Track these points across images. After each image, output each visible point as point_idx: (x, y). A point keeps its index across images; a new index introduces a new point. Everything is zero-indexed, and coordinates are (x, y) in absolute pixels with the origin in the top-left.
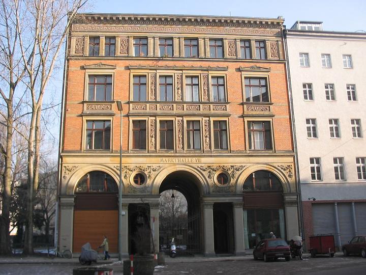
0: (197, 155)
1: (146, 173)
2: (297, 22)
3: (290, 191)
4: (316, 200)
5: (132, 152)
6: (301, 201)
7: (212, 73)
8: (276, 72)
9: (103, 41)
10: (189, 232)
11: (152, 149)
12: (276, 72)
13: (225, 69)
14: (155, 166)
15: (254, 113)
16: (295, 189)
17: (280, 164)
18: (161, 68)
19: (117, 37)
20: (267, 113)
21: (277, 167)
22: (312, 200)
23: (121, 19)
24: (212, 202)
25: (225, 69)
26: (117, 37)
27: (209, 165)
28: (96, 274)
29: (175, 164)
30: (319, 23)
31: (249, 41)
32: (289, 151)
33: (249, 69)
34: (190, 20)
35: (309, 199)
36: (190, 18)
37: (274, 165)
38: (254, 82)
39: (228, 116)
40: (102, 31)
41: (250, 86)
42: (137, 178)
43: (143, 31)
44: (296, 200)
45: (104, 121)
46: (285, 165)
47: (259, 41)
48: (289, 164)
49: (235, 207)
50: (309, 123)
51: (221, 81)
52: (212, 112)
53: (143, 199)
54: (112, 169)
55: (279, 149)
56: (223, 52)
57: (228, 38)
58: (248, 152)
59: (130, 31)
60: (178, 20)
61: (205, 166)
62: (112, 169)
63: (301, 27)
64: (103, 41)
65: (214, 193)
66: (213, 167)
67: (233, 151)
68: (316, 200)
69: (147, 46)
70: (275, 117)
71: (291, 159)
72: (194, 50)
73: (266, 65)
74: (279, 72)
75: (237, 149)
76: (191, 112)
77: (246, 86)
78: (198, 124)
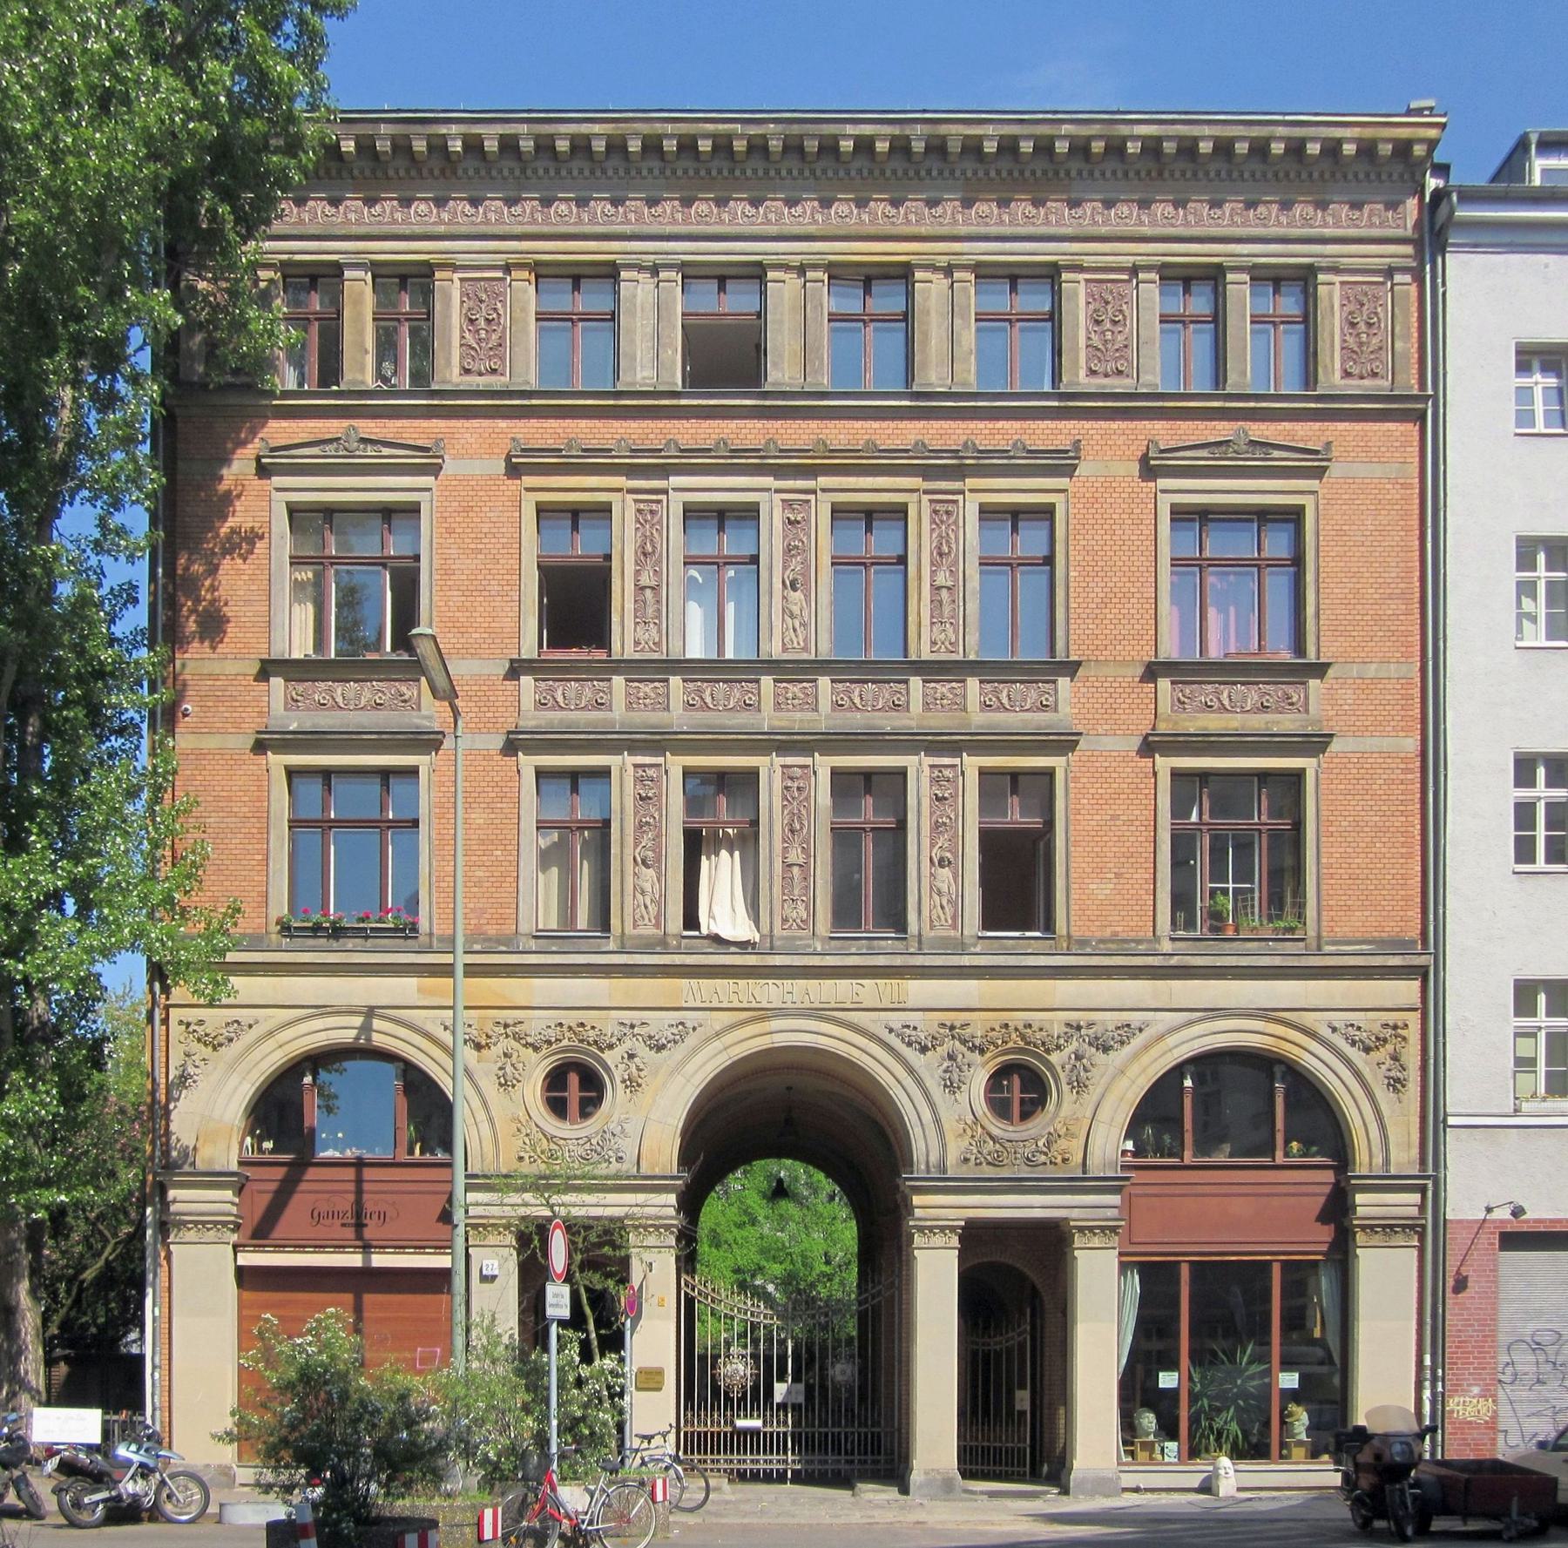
0: (881, 961)
1: (610, 1057)
2: (1522, 146)
3: (1387, 1161)
4: (1529, 1215)
5: (533, 945)
6: (1440, 1223)
7: (974, 495)
8: (1361, 470)
9: (360, 294)
10: (838, 1367)
11: (641, 931)
12: (1361, 470)
13: (1062, 464)
14: (660, 1023)
15: (1213, 723)
16: (1415, 1152)
17: (1338, 1018)
18: (691, 462)
19: (443, 266)
20: (1286, 723)
21: (1325, 1032)
22: (1503, 1214)
23: (457, 146)
24: (958, 1217)
25: (1062, 464)
26: (443, 266)
27: (948, 1017)
28: (411, 1541)
29: (763, 1014)
30: (1516, 435)
31: (1214, 276)
32: (1397, 945)
33: (1202, 458)
34: (864, 146)
35: (1489, 1210)
36: (867, 130)
37: (1308, 1019)
38: (1221, 542)
39: (1065, 744)
40: (355, 230)
41: (1202, 564)
42: (564, 1088)
43: (588, 229)
44: (1414, 1211)
45: (385, 774)
46: (1371, 1023)
47: (1270, 278)
48: (1391, 1017)
49: (1078, 1241)
50: (1531, 783)
51: (1030, 541)
52: (978, 719)
53: (555, 1199)
54: (427, 1036)
55: (1341, 931)
56: (1057, 352)
57: (1088, 261)
58: (1167, 946)
59: (518, 229)
60: (793, 147)
61: (926, 1024)
62: (427, 1036)
63: (1544, 171)
64: (360, 294)
65: (964, 1172)
66: (968, 1031)
67: (1083, 943)
68: (1529, 1215)
69: (616, 335)
70: (1335, 746)
71: (1408, 991)
72: (880, 345)
73: (1306, 433)
74: (1378, 470)
75: (1108, 933)
76: (856, 721)
77: (1175, 562)
78: (603, 331)
